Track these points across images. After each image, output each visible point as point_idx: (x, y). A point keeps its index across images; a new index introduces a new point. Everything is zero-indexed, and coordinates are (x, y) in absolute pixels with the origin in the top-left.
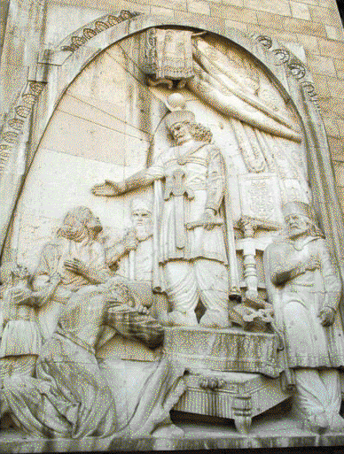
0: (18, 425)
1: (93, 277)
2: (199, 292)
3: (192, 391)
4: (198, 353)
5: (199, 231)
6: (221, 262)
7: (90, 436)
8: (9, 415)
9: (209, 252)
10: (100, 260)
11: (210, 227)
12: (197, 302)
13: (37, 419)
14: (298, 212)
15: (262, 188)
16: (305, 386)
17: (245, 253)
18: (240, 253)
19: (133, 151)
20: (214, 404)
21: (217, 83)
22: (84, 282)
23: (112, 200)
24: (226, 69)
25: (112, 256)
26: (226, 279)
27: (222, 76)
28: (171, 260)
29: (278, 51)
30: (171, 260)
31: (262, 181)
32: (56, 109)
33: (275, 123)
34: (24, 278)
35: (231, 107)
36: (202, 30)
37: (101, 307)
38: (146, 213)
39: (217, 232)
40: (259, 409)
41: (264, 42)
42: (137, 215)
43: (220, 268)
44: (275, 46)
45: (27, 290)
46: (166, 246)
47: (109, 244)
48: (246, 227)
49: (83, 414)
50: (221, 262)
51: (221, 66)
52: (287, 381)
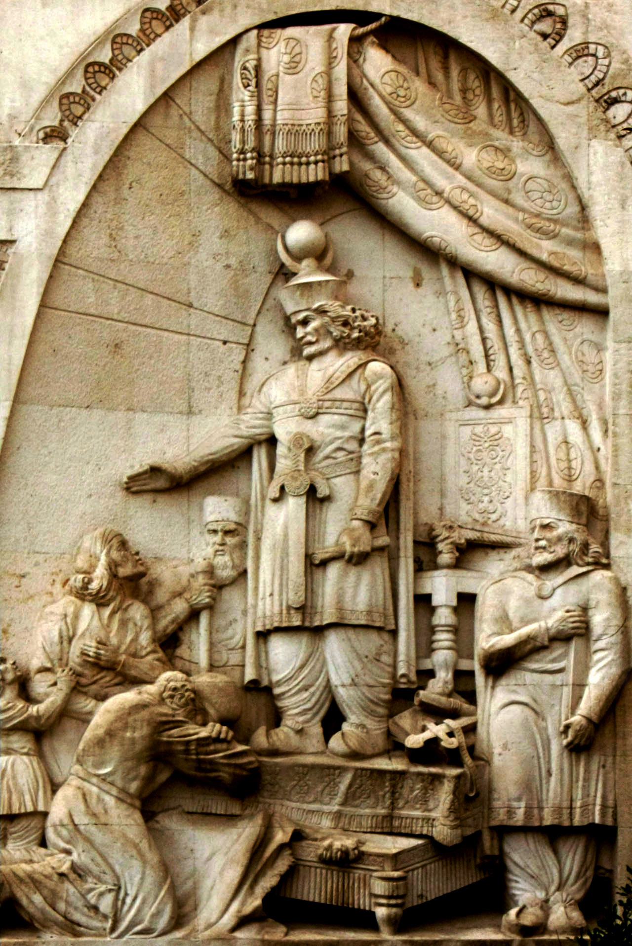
0: (27, 918)
1: (133, 673)
2: (328, 687)
3: (304, 866)
4: (321, 802)
5: (333, 571)
6: (380, 629)
7: (84, 87)
8: (13, 903)
9: (353, 611)
10: (145, 638)
11: (359, 559)
12: (327, 705)
13: (54, 909)
14: (554, 514)
15: (492, 448)
16: (516, 857)
17: (435, 601)
18: (423, 602)
19: (207, 374)
20: (344, 891)
21: (405, 174)
22: (116, 681)
23: (162, 499)
24: (434, 131)
25: (165, 622)
26: (386, 659)
27: (421, 155)
28: (278, 630)
29: (580, 52)
30: (278, 630)
31: (493, 429)
32: (44, 305)
33: (542, 275)
34: (12, 682)
35: (436, 240)
36: (377, 16)
37: (145, 731)
38: (232, 526)
39: (378, 568)
40: (421, 896)
41: (545, 26)
42: (215, 532)
43: (372, 642)
44: (574, 36)
45: (20, 704)
46: (268, 599)
47: (161, 596)
48: (441, 546)
49: (124, 902)
50: (380, 629)
51: (420, 123)
52: (483, 851)
